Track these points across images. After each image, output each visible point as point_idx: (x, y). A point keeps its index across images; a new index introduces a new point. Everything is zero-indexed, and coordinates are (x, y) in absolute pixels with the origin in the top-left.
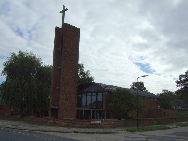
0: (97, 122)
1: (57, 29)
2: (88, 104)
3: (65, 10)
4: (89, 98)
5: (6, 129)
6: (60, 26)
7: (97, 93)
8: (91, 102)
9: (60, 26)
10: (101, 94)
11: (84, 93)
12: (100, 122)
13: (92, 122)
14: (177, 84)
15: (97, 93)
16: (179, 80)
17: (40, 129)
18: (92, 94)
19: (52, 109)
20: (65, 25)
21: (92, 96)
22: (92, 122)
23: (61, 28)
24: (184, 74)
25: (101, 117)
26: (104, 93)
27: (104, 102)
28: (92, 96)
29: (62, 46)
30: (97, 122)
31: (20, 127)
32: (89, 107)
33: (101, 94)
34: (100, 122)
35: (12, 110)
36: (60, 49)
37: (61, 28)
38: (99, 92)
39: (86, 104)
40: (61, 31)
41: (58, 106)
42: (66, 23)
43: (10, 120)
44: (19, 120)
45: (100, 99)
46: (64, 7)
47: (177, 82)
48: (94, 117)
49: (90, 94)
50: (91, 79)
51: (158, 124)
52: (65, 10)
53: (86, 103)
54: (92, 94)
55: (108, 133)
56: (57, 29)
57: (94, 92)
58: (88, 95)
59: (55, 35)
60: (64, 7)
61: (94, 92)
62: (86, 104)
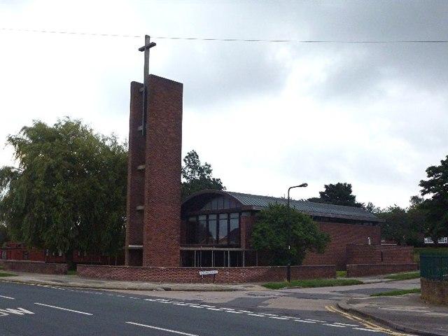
0: (209, 272)
1: (135, 86)
2: (221, 237)
3: (147, 47)
4: (224, 224)
5: (46, 286)
6: (141, 81)
7: (229, 212)
8: (229, 228)
9: (141, 81)
10: (214, 217)
11: (203, 214)
12: (217, 272)
13: (201, 273)
14: (422, 188)
15: (229, 212)
16: (427, 179)
17: (107, 286)
18: (218, 216)
19: (131, 250)
20: (152, 80)
21: (229, 219)
22: (201, 273)
23: (143, 82)
24: (438, 164)
25: (219, 263)
26: (243, 214)
27: (243, 235)
28: (229, 219)
29: (145, 122)
30: (209, 272)
31: (71, 283)
32: (225, 243)
33: (237, 215)
34: (217, 272)
35: (60, 255)
36: (141, 128)
37: (126, 149)
38: (234, 211)
39: (218, 236)
40: (142, 89)
41: (142, 244)
42: (152, 76)
43: (49, 273)
44: (65, 273)
45: (235, 224)
46: (147, 37)
47: (423, 184)
48: (206, 264)
49: (214, 217)
50: (217, 184)
51: (348, 276)
52: (147, 47)
53: (218, 233)
54: (218, 216)
55: (225, 291)
56: (135, 86)
57: (223, 212)
58: (210, 218)
59: (130, 116)
60: (147, 37)
61: (223, 212)
62: (218, 236)
